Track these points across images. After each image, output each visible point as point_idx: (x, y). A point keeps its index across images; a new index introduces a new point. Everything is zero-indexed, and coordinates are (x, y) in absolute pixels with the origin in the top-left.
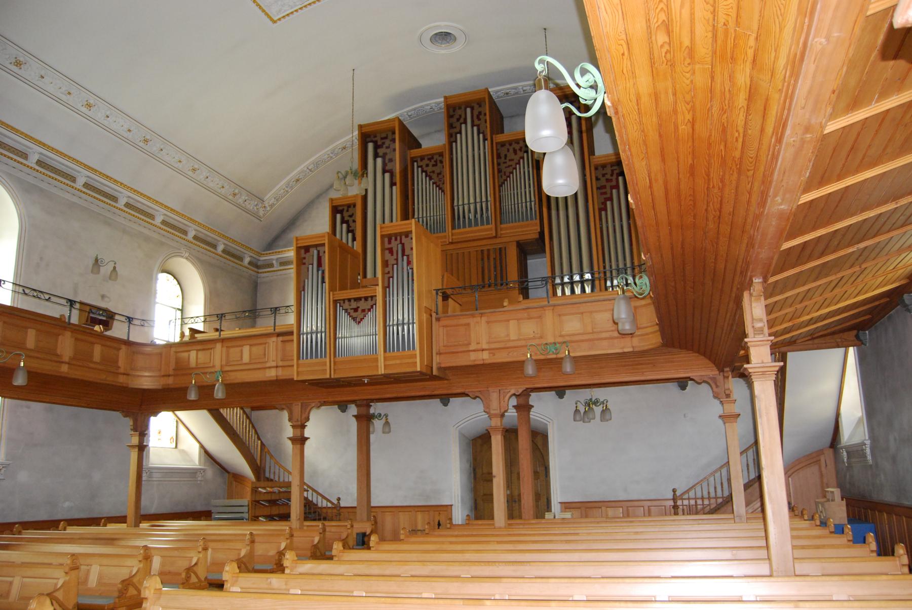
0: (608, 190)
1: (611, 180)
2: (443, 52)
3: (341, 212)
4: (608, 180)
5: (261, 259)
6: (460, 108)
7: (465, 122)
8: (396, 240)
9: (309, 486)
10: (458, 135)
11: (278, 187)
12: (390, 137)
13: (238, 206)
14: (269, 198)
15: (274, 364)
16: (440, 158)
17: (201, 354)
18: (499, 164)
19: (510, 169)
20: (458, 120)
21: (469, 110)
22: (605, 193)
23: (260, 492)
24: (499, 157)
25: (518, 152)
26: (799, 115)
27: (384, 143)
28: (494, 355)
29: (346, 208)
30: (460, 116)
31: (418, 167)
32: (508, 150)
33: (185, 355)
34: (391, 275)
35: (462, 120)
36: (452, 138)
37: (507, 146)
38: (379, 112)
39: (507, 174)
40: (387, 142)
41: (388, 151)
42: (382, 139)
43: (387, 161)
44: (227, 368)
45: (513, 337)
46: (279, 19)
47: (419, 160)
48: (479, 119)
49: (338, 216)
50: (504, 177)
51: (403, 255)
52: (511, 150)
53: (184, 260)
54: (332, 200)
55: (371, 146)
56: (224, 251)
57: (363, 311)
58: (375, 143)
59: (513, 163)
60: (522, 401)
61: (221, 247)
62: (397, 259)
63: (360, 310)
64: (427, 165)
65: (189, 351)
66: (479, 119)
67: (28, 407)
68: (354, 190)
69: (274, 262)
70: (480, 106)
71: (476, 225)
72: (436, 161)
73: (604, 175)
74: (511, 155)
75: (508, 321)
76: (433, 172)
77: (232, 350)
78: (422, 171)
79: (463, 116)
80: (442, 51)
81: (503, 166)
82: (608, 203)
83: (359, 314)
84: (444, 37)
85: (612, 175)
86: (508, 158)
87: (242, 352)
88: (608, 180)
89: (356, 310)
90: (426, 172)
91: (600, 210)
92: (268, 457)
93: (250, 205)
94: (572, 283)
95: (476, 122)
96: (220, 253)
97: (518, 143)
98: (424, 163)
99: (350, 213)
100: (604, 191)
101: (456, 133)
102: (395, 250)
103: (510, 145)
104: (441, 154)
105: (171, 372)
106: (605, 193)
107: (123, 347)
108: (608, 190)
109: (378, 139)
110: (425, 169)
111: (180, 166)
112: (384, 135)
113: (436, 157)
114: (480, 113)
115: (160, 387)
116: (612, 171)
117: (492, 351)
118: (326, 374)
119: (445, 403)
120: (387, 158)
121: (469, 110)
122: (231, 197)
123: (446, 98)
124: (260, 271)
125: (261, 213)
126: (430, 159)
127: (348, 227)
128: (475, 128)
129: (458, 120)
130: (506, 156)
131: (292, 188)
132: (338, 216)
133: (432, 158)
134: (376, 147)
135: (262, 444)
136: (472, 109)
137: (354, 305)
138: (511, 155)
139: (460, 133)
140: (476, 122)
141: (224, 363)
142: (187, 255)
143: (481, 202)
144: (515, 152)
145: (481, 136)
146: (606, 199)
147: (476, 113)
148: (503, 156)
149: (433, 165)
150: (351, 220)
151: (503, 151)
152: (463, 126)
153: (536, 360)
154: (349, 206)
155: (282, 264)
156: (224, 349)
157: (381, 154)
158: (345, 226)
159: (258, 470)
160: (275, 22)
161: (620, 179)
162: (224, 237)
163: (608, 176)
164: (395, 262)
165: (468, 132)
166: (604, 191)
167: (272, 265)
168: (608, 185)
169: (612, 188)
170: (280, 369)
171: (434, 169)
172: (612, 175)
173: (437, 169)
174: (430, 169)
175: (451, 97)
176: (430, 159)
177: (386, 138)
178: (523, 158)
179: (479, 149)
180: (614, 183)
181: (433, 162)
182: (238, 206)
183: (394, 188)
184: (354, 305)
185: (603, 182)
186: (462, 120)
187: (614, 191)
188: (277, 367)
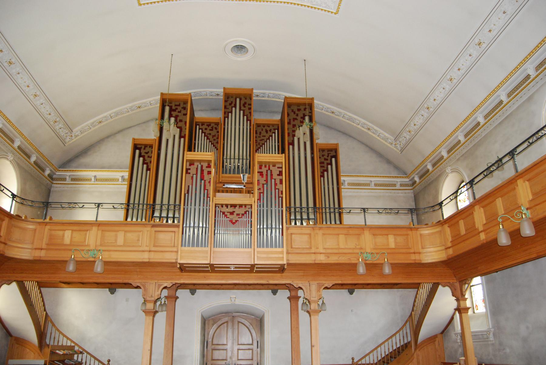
0: (325, 165)
1: (327, 160)
2: (239, 59)
3: (140, 149)
4: (326, 159)
5: (57, 173)
6: (232, 97)
7: (235, 106)
8: (265, 166)
9: (84, 350)
10: (230, 114)
11: (85, 124)
12: (182, 106)
13: (54, 131)
14: (76, 130)
15: (147, 249)
16: (216, 126)
17: (76, 234)
18: (256, 137)
19: (263, 142)
20: (230, 104)
21: (238, 100)
22: (323, 167)
23: (57, 353)
24: (256, 133)
25: (269, 132)
26: (68, 174)
27: (177, 109)
28: (328, 257)
29: (143, 147)
30: (232, 102)
31: (199, 129)
32: (262, 130)
33: (61, 233)
34: (262, 191)
35: (233, 105)
36: (226, 116)
37: (262, 127)
38: (176, 89)
39: (261, 144)
40: (179, 108)
41: (179, 114)
42: (176, 105)
43: (178, 121)
44: (100, 248)
45: (342, 246)
46: (144, 4)
47: (200, 124)
48: (245, 107)
49: (137, 152)
50: (259, 146)
51: (272, 178)
52: (264, 130)
53: (8, 162)
54: (134, 139)
55: (167, 109)
56: (35, 163)
57: (238, 215)
58: (171, 108)
59: (265, 138)
60: (172, 292)
61: (33, 159)
62: (266, 181)
63: (235, 214)
64: (206, 129)
65: (65, 230)
66: (245, 107)
67: (149, 259)
68: (150, 134)
69: (68, 177)
70: (246, 99)
71: (230, 173)
72: (212, 128)
73: (323, 156)
74: (264, 133)
75: (338, 234)
76: (210, 134)
77: (107, 234)
78: (202, 132)
79: (234, 103)
80: (240, 58)
81: (258, 139)
82: (325, 173)
83: (234, 218)
84: (240, 48)
85: (328, 156)
86: (262, 135)
87: (116, 236)
88: (326, 159)
89: (232, 213)
90: (205, 133)
91: (321, 176)
92: (50, 325)
93: (62, 133)
94: (309, 219)
95: (243, 108)
96: (33, 163)
97: (269, 127)
98: (204, 127)
99: (146, 151)
100: (323, 165)
101: (228, 113)
102: (265, 174)
103: (264, 127)
104: (217, 124)
105: (44, 246)
106: (323, 167)
107: (7, 219)
108: (325, 165)
109: (173, 105)
110: (204, 131)
111: (27, 89)
112: (178, 104)
113: (212, 125)
114: (245, 103)
115: (31, 258)
116: (328, 154)
117: (328, 255)
118: (283, 260)
119: (112, 292)
120: (179, 119)
121: (238, 100)
122: (52, 123)
123: (224, 88)
124: (54, 182)
125: (67, 140)
126: (208, 125)
127: (144, 160)
128: (242, 112)
129: (230, 104)
130: (260, 133)
131: (94, 126)
132: (137, 152)
133: (210, 125)
134: (171, 110)
135: (47, 314)
136: (240, 100)
137: (231, 209)
138: (264, 133)
139: (231, 112)
140: (243, 108)
141: (99, 243)
142: (12, 159)
143: (243, 159)
144: (267, 131)
145: (245, 117)
146: (324, 171)
147: (242, 102)
148: (258, 132)
149: (210, 130)
150: (146, 156)
151: (259, 130)
152: (234, 109)
153: (391, 264)
154: (146, 146)
155: (73, 180)
156: (100, 233)
157: (174, 115)
158: (141, 159)
159: (41, 335)
160: (140, 5)
161: (333, 160)
162: (38, 152)
163: (326, 157)
164: (265, 182)
165: (237, 114)
166: (323, 165)
167: (65, 179)
168: (326, 162)
169: (328, 164)
170: (152, 253)
171: (211, 132)
172: (328, 156)
173: (214, 132)
174: (208, 132)
175: (228, 89)
176: (208, 125)
177: (179, 105)
178: (272, 136)
179: (243, 125)
180: (329, 162)
181: (210, 128)
182: (54, 131)
183: (182, 139)
184: (231, 209)
185: (323, 160)
186: (233, 105)
187: (329, 166)
188: (150, 251)
